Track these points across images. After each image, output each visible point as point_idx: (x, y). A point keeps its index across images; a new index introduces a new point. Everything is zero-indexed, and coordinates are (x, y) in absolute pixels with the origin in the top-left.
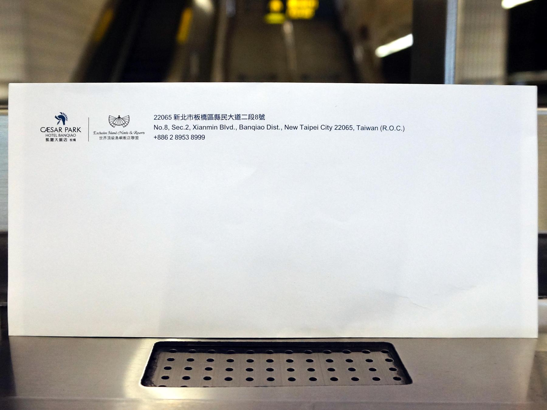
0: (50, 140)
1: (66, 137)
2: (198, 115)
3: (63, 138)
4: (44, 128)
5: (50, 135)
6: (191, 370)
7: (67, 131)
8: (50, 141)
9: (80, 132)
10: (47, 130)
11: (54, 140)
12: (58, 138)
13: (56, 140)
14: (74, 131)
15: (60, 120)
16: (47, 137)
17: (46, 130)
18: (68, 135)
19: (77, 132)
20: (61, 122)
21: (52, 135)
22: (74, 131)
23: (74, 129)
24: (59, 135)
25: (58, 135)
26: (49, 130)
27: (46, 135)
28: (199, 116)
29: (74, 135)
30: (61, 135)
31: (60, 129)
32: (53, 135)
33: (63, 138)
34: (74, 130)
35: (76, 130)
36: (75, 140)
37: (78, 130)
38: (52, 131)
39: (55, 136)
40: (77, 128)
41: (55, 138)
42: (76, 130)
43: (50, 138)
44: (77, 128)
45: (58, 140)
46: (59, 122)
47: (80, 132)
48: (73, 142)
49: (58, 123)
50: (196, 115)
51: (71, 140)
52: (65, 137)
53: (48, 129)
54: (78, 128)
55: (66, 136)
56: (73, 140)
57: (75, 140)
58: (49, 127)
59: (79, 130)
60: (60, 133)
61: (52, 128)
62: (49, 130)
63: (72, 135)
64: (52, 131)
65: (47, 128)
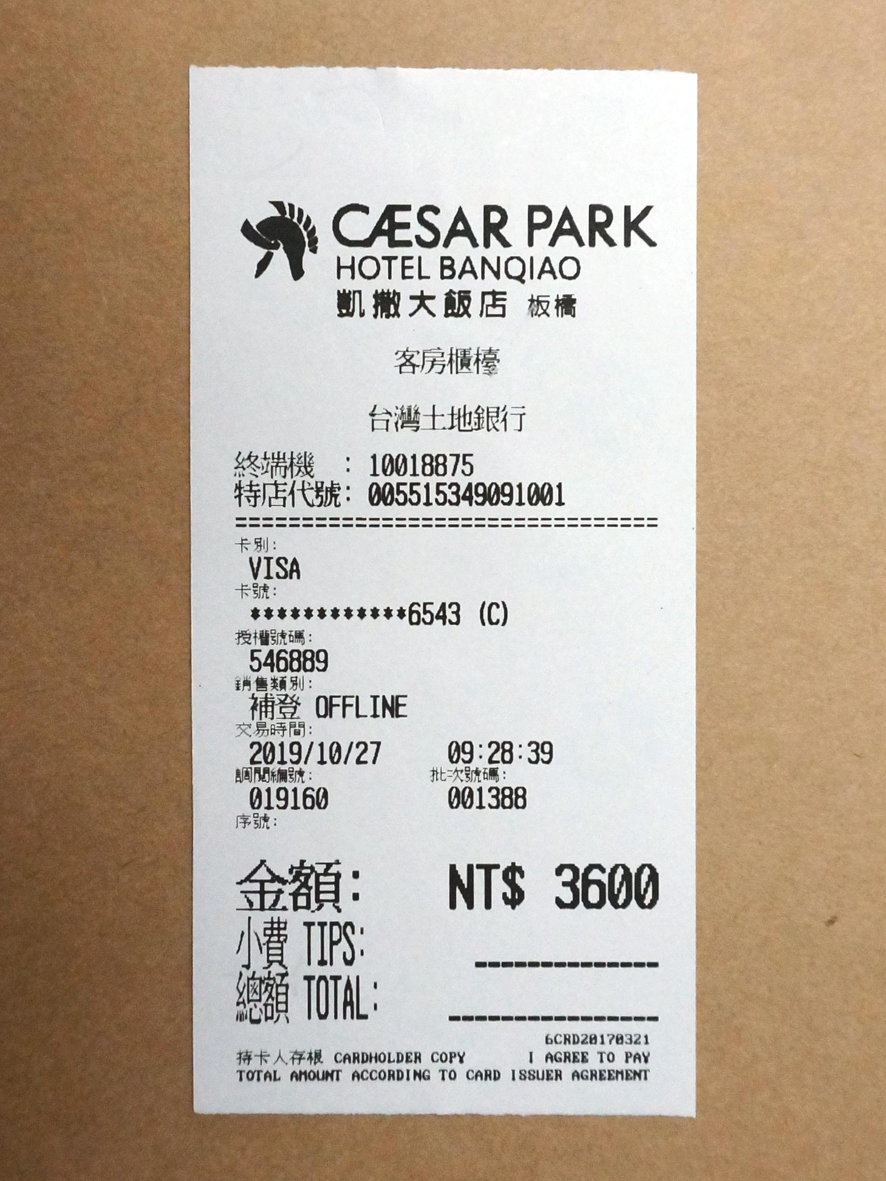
0: (368, 303)
1: (503, 284)
2: (540, 299)
3: (474, 286)
4: (365, 210)
5: (369, 268)
6: (250, 660)
7: (543, 236)
8: (370, 310)
9: (652, 244)
10: (385, 226)
11: (406, 305)
12: (438, 288)
13: (422, 305)
14: (598, 238)
15: (276, 247)
16: (347, 283)
17: (378, 231)
18: (515, 268)
19: (627, 243)
20: (280, 256)
21: (384, 264)
22: (598, 238)
23: (600, 217)
24: (447, 266)
25: (432, 267)
26: (406, 226)
27: (339, 267)
28: (548, 302)
29: (570, 268)
30: (458, 268)
31: (495, 217)
32: (397, 265)
33: (474, 286)
34: (596, 228)
35: (616, 230)
36: (567, 305)
37: (631, 226)
38: (428, 236)
39: (414, 272)
40: (627, 209)
41: (407, 289)
42: (616, 230)
43: (368, 290)
44: (627, 209)
45: (438, 305)
46: (267, 259)
47: (652, 244)
48: (555, 321)
49: (262, 266)
50: (535, 298)
51: (536, 302)
52: (490, 283)
53: (399, 217)
54: (633, 217)
55: (497, 275)
56: (552, 310)
57: (567, 305)
58: (407, 208)
59: (642, 225)
60: (495, 250)
61: (428, 216)
62: (406, 226)
63: (547, 268)
64: (428, 236)
65: (390, 211)
